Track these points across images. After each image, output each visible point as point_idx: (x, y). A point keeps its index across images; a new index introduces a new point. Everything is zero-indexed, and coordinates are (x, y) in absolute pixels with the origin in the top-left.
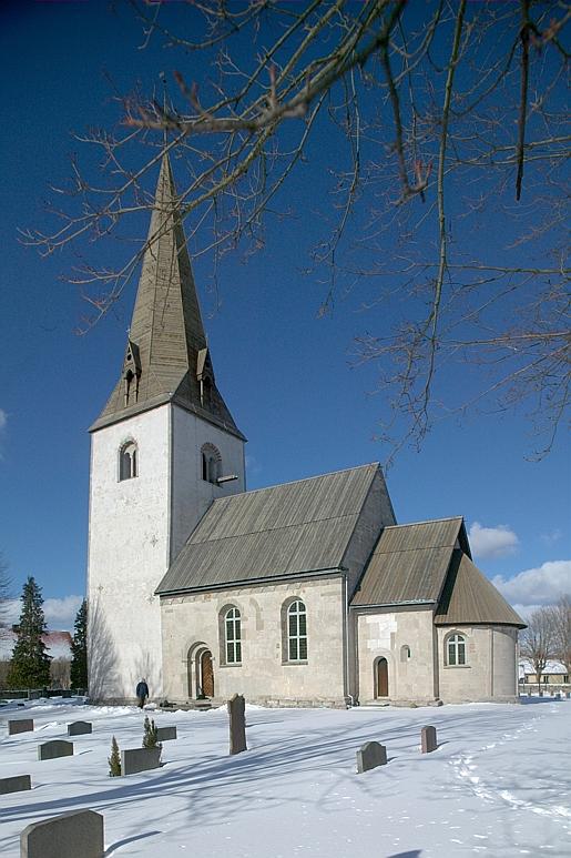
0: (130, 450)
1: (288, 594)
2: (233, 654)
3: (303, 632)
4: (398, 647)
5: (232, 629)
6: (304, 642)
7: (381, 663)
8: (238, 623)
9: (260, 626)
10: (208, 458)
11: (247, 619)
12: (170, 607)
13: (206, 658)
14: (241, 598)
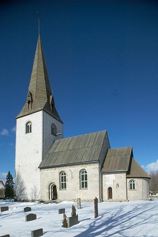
0: (29, 124)
1: (82, 168)
2: (64, 186)
3: (65, 181)
4: (115, 184)
5: (63, 178)
6: (65, 184)
7: (110, 189)
8: (65, 177)
9: (72, 178)
10: (53, 128)
11: (68, 176)
12: (43, 172)
13: (55, 187)
14: (66, 169)
